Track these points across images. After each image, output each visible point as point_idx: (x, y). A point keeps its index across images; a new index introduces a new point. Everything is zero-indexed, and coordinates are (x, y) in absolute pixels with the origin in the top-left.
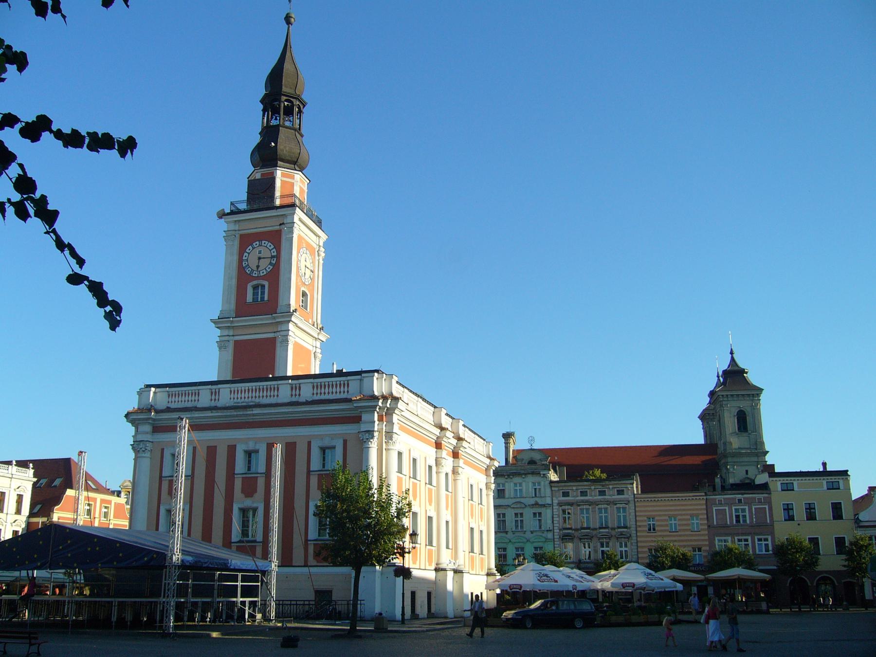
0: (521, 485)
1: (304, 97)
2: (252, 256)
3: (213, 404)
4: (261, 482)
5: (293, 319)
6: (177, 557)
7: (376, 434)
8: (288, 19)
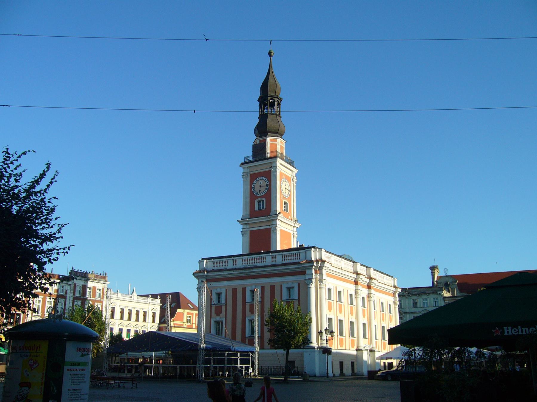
0: (426, 299)
1: (281, 96)
2: (256, 185)
3: (234, 267)
4: (223, 308)
5: (278, 218)
6: (203, 345)
7: (314, 280)
8: (270, 54)
